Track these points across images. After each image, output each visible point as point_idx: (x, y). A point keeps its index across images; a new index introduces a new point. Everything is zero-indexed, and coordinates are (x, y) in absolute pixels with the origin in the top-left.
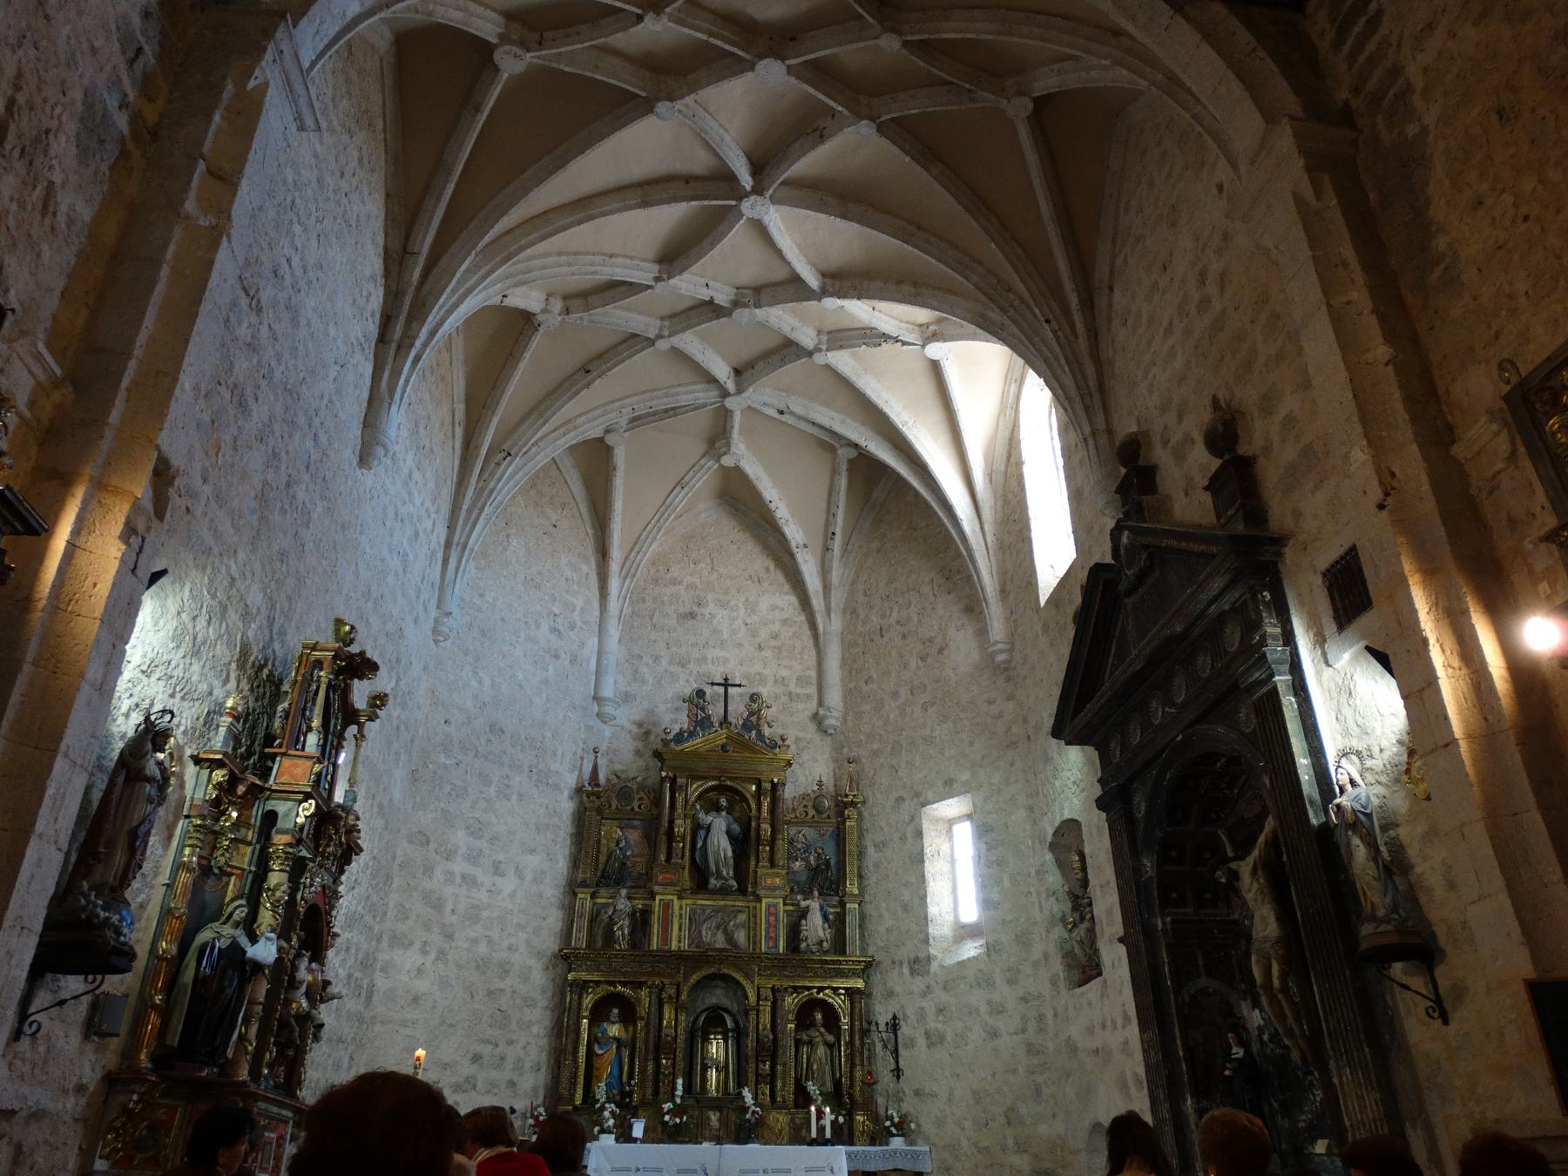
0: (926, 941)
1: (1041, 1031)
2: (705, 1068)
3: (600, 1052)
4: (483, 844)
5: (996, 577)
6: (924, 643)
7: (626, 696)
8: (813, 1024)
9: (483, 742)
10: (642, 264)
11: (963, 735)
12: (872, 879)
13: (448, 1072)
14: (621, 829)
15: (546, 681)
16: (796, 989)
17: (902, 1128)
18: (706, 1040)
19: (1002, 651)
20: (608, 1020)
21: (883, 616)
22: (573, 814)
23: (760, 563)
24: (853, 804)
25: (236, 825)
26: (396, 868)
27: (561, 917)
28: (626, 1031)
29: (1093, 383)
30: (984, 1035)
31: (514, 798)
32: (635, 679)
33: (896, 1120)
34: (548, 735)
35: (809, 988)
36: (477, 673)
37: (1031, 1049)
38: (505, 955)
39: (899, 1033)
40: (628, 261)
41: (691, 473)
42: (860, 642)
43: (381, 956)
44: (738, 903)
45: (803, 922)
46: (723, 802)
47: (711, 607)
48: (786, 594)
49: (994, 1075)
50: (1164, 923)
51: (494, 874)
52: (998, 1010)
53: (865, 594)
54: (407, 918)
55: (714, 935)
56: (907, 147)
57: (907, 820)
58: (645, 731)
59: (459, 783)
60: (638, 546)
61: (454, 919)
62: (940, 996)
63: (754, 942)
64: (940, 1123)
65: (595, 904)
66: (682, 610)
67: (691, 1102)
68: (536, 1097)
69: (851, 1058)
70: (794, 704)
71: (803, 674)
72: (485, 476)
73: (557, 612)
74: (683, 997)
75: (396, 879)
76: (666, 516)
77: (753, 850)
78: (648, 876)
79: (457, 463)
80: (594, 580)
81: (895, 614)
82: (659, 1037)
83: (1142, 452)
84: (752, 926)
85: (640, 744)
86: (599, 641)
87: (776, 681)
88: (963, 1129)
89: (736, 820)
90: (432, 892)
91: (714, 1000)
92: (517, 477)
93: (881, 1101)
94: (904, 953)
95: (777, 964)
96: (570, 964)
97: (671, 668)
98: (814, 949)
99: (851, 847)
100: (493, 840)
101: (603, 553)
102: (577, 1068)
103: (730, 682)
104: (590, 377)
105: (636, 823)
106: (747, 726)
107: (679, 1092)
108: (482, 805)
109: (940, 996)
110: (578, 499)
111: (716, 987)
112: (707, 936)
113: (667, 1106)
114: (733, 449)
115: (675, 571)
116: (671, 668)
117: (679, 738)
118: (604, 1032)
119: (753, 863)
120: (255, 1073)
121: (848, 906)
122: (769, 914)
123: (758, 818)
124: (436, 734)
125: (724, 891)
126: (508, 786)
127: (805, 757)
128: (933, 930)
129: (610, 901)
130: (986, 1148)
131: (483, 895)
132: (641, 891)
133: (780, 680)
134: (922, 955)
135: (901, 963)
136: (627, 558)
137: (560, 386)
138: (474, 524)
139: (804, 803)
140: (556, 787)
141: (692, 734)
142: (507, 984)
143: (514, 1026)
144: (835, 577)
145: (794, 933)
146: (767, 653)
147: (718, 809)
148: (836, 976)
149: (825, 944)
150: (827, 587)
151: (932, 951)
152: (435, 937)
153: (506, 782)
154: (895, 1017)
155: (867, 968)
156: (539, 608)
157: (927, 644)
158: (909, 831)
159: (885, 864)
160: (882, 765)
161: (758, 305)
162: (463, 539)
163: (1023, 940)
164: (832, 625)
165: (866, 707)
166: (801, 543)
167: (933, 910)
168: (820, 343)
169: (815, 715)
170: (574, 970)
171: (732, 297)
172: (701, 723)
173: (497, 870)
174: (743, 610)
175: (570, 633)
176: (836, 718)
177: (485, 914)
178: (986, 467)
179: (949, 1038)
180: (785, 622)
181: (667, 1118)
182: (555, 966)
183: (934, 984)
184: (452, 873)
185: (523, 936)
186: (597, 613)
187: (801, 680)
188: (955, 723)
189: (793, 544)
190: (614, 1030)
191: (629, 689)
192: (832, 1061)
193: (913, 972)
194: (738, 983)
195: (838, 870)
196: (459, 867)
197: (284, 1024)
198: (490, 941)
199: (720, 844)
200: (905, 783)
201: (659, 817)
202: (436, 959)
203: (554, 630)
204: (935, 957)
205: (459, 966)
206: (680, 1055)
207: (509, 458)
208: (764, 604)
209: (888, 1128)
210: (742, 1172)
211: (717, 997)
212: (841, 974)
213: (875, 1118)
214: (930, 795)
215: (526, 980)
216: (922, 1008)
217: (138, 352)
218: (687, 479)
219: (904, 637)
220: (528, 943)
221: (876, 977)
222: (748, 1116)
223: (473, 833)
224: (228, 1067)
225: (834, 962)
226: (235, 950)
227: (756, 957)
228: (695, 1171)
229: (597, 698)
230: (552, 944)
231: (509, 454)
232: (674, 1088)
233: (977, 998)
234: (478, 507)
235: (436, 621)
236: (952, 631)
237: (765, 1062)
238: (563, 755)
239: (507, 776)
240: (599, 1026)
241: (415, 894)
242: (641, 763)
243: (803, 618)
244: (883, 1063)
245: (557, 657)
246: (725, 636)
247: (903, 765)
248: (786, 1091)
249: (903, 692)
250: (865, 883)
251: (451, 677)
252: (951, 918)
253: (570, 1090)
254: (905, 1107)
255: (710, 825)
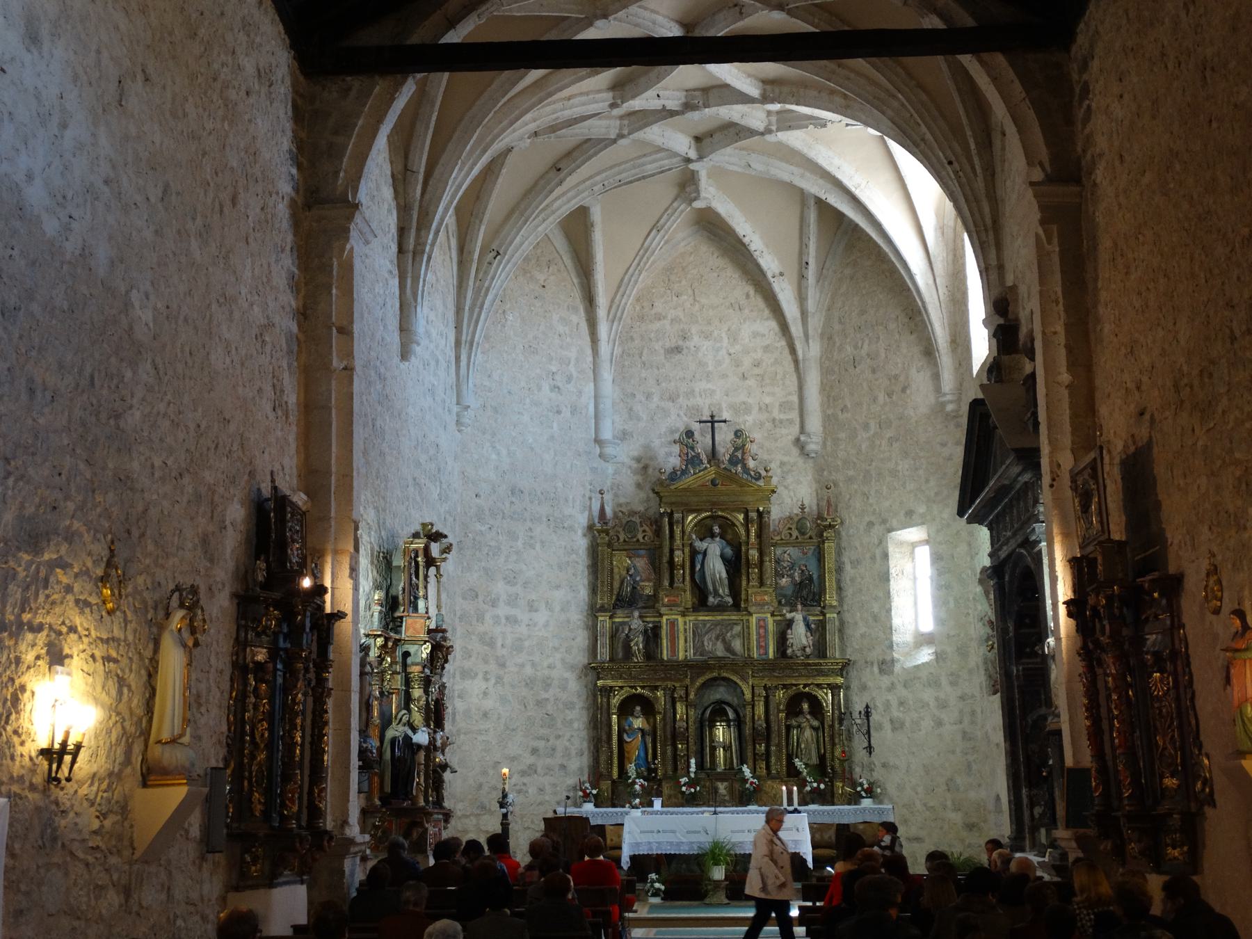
0: (891, 647)
1: (973, 722)
2: (713, 749)
3: (629, 740)
4: (518, 589)
5: (947, 329)
6: (890, 379)
7: (624, 434)
8: (800, 712)
9: (507, 504)
10: (597, 96)
11: (921, 472)
12: (849, 592)
13: (515, 763)
14: (630, 558)
15: (552, 438)
16: (785, 686)
17: (870, 792)
18: (712, 726)
19: (951, 402)
20: (632, 715)
21: (856, 347)
22: (588, 549)
23: (740, 289)
24: (830, 526)
25: (391, 665)
26: (457, 621)
27: (586, 636)
28: (648, 723)
29: (989, 221)
30: (932, 723)
31: (538, 546)
32: (631, 418)
33: (866, 786)
34: (560, 485)
35: (796, 685)
36: (494, 447)
37: (965, 736)
38: (546, 672)
39: (871, 718)
40: (584, 98)
41: (665, 217)
42: (836, 369)
43: (456, 687)
44: (733, 617)
45: (789, 631)
46: (716, 529)
47: (696, 340)
48: (767, 319)
49: (939, 754)
50: (1018, 670)
51: (530, 611)
52: (943, 705)
53: (840, 322)
54: (470, 656)
55: (714, 644)
56: (816, 21)
57: (876, 542)
58: (644, 465)
59: (493, 543)
60: (622, 289)
61: (504, 652)
62: (902, 692)
63: (749, 649)
64: (901, 788)
65: (613, 623)
66: (668, 345)
67: (703, 776)
68: (582, 774)
69: (832, 738)
70: (778, 430)
71: (784, 400)
72: (480, 276)
73: (554, 370)
74: (692, 696)
75: (459, 629)
76: (645, 258)
77: (743, 571)
78: (655, 598)
79: (455, 268)
80: (584, 326)
81: (866, 346)
82: (675, 728)
83: (1010, 309)
84: (745, 635)
85: (639, 478)
86: (595, 385)
87: (760, 409)
88: (917, 793)
89: (729, 543)
90: (486, 633)
91: (718, 696)
92: (507, 269)
93: (858, 770)
94: (875, 655)
95: (768, 667)
96: (598, 673)
97: (663, 404)
98: (799, 654)
99: (830, 564)
100: (526, 584)
101: (590, 299)
102: (612, 752)
103: (716, 419)
104: (562, 175)
105: (643, 552)
106: (734, 461)
107: (693, 768)
108: (514, 557)
109: (902, 692)
110: (562, 253)
111: (718, 685)
112: (708, 646)
113: (684, 780)
114: (703, 194)
115: (659, 307)
116: (663, 404)
117: (674, 476)
118: (630, 725)
119: (744, 583)
120: (426, 801)
121: (828, 616)
122: (759, 627)
123: (747, 543)
124: (470, 508)
125: (720, 608)
126: (531, 537)
127: (790, 480)
128: (896, 638)
129: (626, 620)
130: (932, 807)
131: (523, 629)
132: (651, 610)
133: (764, 407)
134: (888, 658)
135: (872, 664)
136: (612, 301)
137: (536, 184)
138: (476, 326)
139: (789, 526)
140: (571, 528)
141: (684, 472)
142: (549, 694)
143: (559, 725)
144: (811, 305)
145: (782, 640)
146: (751, 382)
147: (713, 536)
148: (818, 675)
149: (808, 650)
150: (804, 314)
151: (896, 655)
152: (492, 667)
153: (529, 534)
154: (867, 707)
155: (844, 668)
156: (538, 371)
157: (893, 381)
158: (878, 552)
159: (859, 580)
160: (856, 491)
161: (706, 106)
162: (469, 338)
163: (962, 652)
164: (812, 351)
165: (842, 435)
166: (777, 272)
167: (896, 621)
168: (770, 124)
169: (798, 440)
170: (602, 679)
171: (683, 100)
172: (692, 461)
173: (532, 608)
174: (726, 340)
175: (568, 386)
176: (817, 443)
177: (527, 644)
178: (938, 221)
179: (907, 724)
180: (766, 349)
181: (684, 789)
182: (586, 676)
183: (896, 681)
184: (498, 617)
185: (558, 656)
186: (590, 359)
187: (784, 406)
188: (914, 459)
189: (769, 275)
190: (638, 723)
191: (626, 427)
192: (818, 741)
193: (881, 671)
194: (736, 683)
195: (820, 584)
196: (503, 610)
197: (435, 771)
198: (533, 665)
199: (716, 567)
200: (875, 510)
201: (661, 547)
202: (495, 684)
203: (556, 388)
204: (898, 660)
205: (513, 686)
206: (691, 741)
207: (498, 257)
208: (746, 331)
209: (859, 792)
210: (732, 832)
211: (720, 693)
212: (821, 673)
213: (854, 784)
214: (894, 523)
215: (564, 688)
216: (888, 701)
217: (334, 469)
218: (662, 221)
219: (874, 371)
220: (563, 660)
221: (853, 673)
222: (748, 786)
223: (509, 582)
224: (414, 800)
225: (815, 665)
226: (407, 739)
227: (748, 662)
228: (699, 832)
229: (598, 441)
230: (582, 659)
231: (498, 253)
232: (689, 766)
233: (928, 695)
234: (478, 305)
235: (458, 415)
236: (913, 371)
237: (760, 745)
238: (574, 501)
239: (530, 529)
240: (626, 719)
241: (473, 637)
242: (642, 495)
243: (783, 343)
244: (859, 742)
245: (559, 412)
246: (710, 368)
247: (872, 493)
248: (778, 765)
249: (873, 424)
250: (844, 594)
251: (476, 457)
252: (911, 628)
253: (608, 768)
254: (876, 775)
255: (706, 550)
